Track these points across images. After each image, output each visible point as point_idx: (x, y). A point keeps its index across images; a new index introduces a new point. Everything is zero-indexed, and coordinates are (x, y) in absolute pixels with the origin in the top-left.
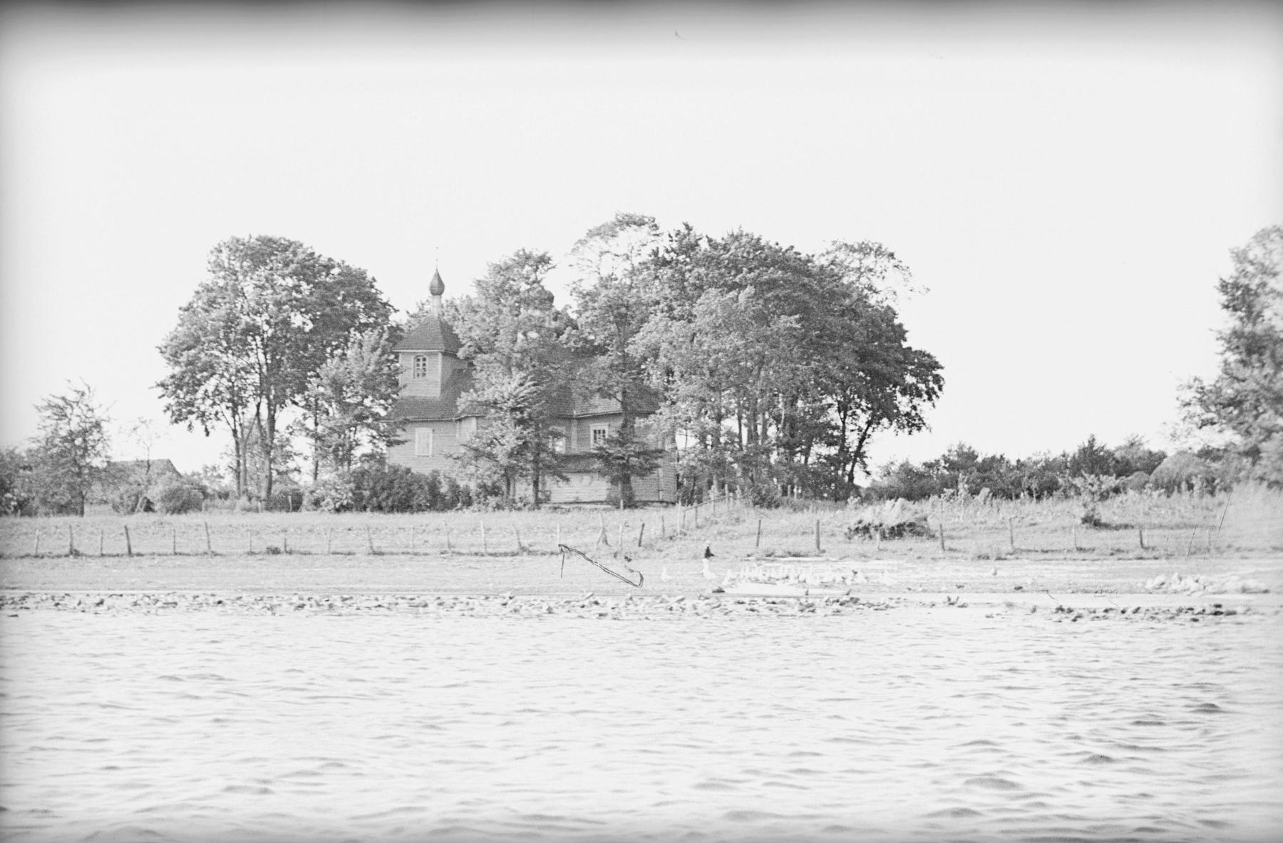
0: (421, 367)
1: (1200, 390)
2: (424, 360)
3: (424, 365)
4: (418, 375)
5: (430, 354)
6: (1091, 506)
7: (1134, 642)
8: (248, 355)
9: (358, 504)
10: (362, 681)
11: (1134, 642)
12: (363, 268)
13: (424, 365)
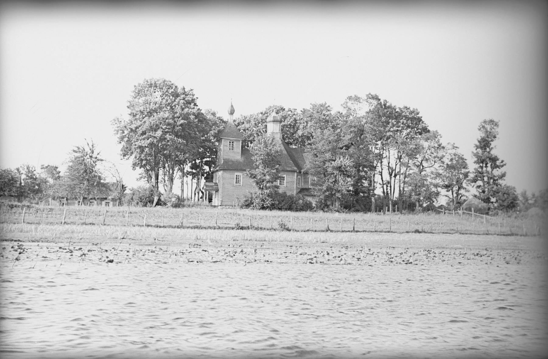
0: (231, 146)
1: (251, 138)
2: (233, 143)
3: (233, 145)
4: (230, 149)
5: (236, 140)
6: (230, 239)
7: (411, 332)
8: (406, 145)
9: (272, 207)
10: (53, 282)
11: (411, 332)
12: (319, 101)
13: (233, 145)
